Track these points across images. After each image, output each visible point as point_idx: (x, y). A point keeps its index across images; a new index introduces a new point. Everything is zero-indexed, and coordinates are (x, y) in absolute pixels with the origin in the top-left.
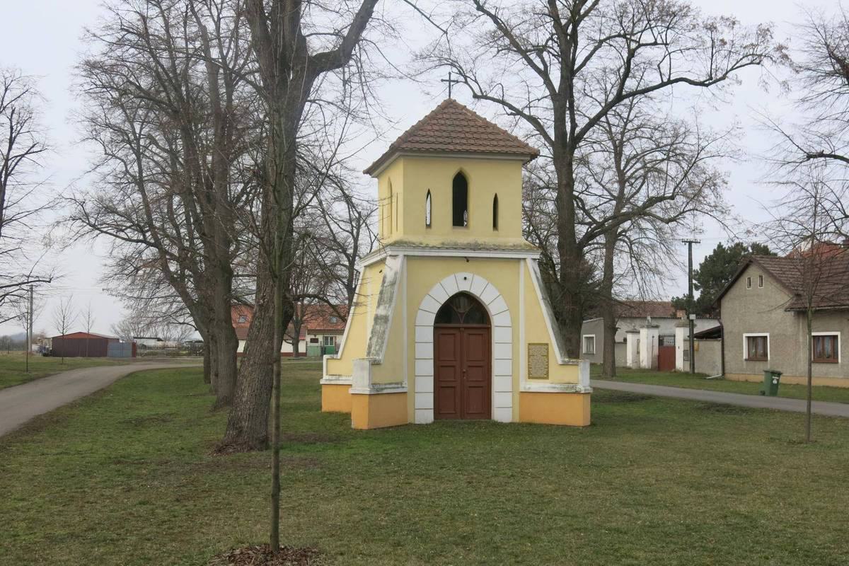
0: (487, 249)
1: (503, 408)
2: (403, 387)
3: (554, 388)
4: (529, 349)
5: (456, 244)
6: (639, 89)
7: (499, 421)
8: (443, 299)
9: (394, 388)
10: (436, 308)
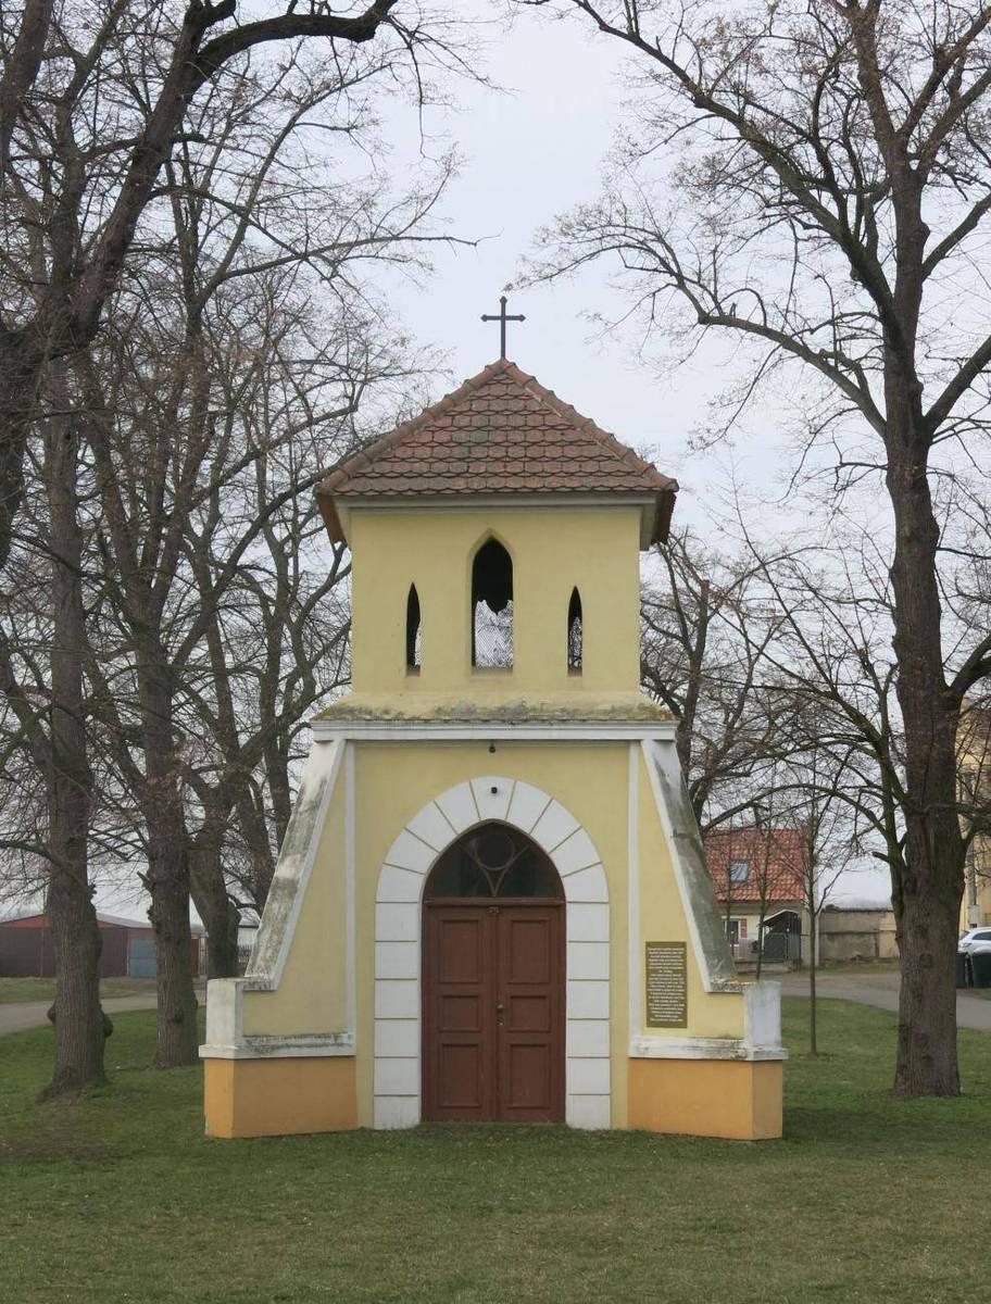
1: (591, 1095)
2: (342, 1045)
3: (695, 1048)
4: (648, 956)
5: (470, 711)
6: (876, 313)
7: (592, 1129)
9: (316, 1046)
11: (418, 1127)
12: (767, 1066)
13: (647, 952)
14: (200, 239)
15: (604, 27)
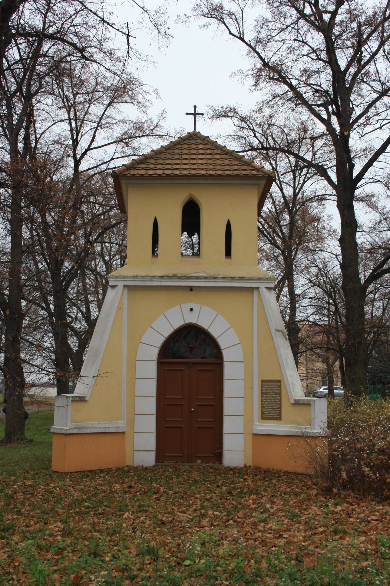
0: (179, 277)
1: (235, 449)
4: (262, 386)
8: (214, 331)
10: (159, 341)
11: (154, 466)
13: (262, 384)
15: (230, 33)
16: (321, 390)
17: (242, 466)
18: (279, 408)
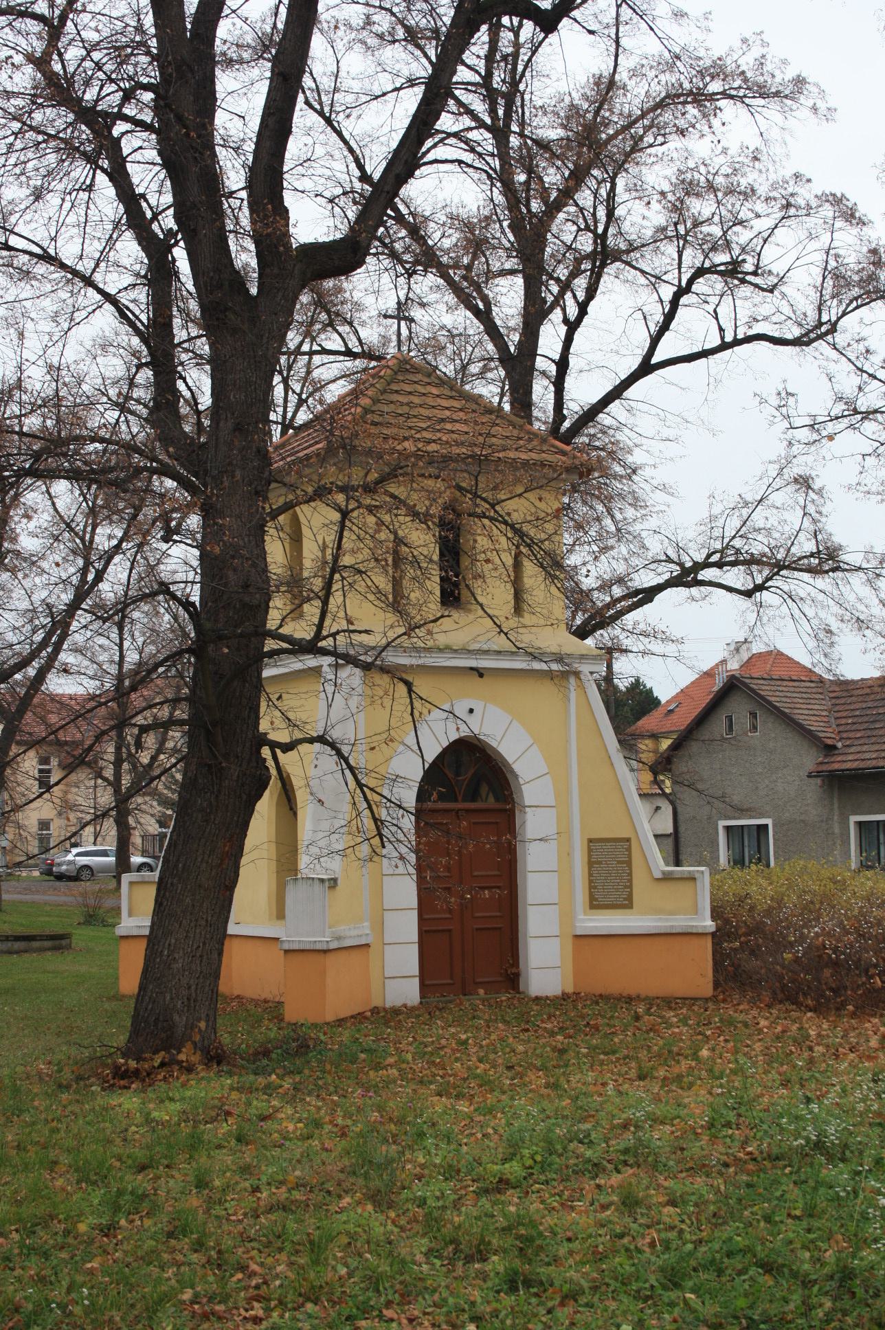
0: (456, 651)
1: (546, 966)
4: (590, 850)
12: (258, 942)
13: (589, 847)
14: (424, 149)
16: (70, 857)
17: (559, 992)
18: (626, 887)
